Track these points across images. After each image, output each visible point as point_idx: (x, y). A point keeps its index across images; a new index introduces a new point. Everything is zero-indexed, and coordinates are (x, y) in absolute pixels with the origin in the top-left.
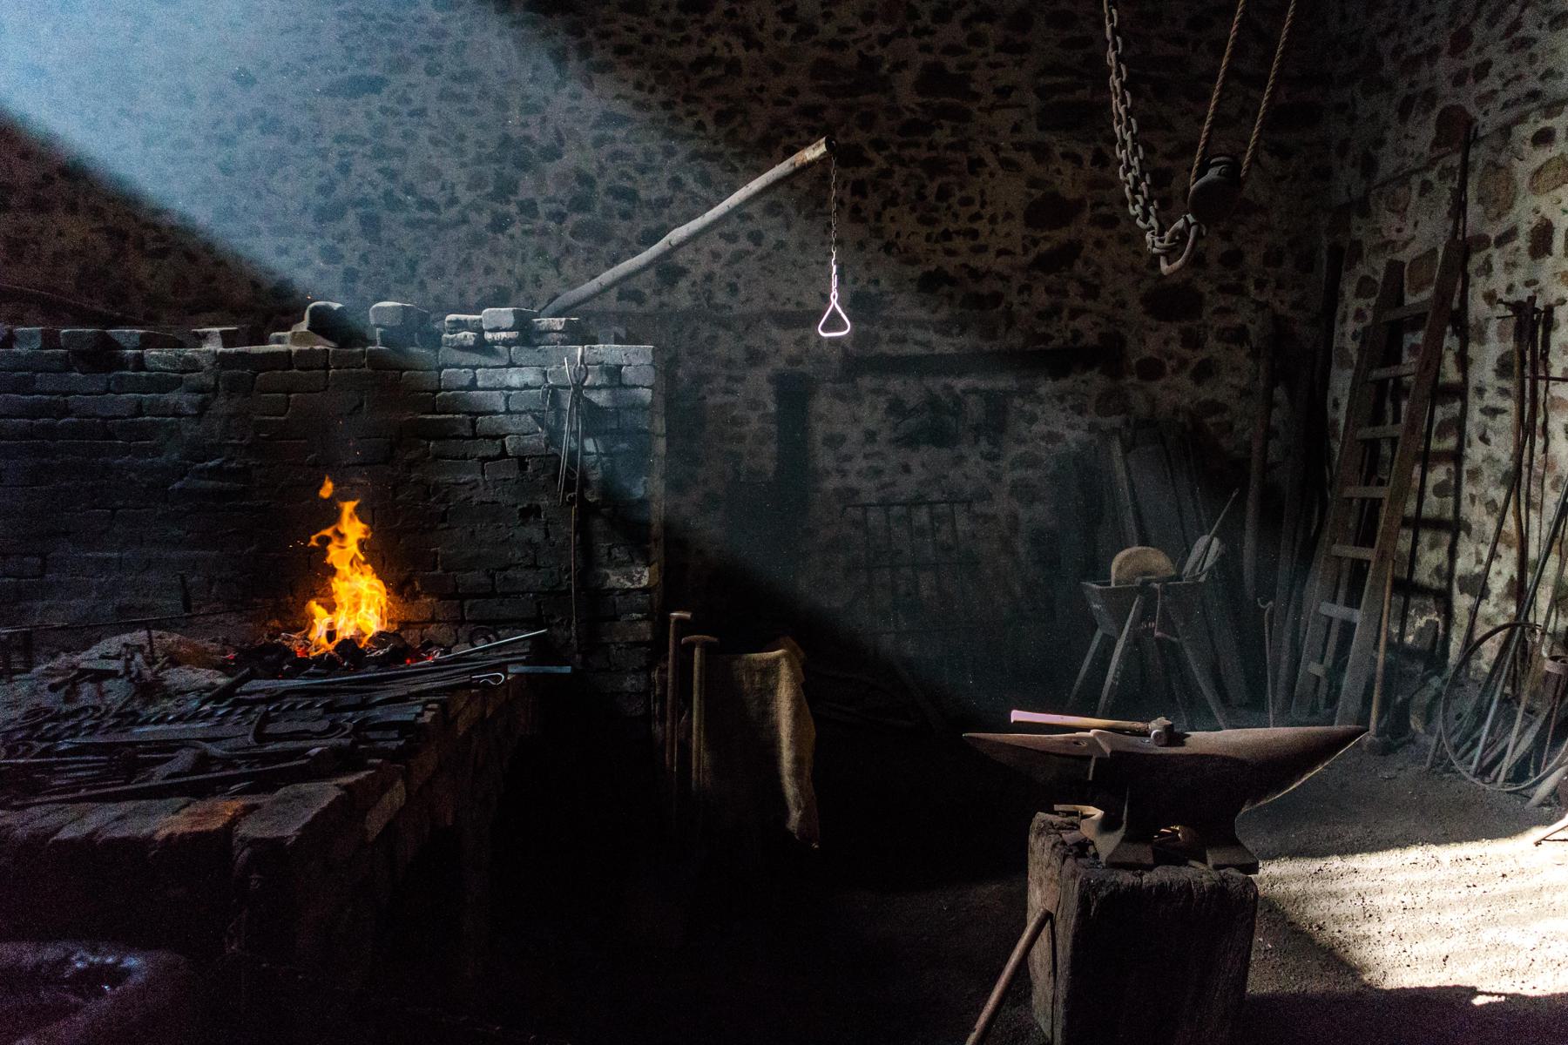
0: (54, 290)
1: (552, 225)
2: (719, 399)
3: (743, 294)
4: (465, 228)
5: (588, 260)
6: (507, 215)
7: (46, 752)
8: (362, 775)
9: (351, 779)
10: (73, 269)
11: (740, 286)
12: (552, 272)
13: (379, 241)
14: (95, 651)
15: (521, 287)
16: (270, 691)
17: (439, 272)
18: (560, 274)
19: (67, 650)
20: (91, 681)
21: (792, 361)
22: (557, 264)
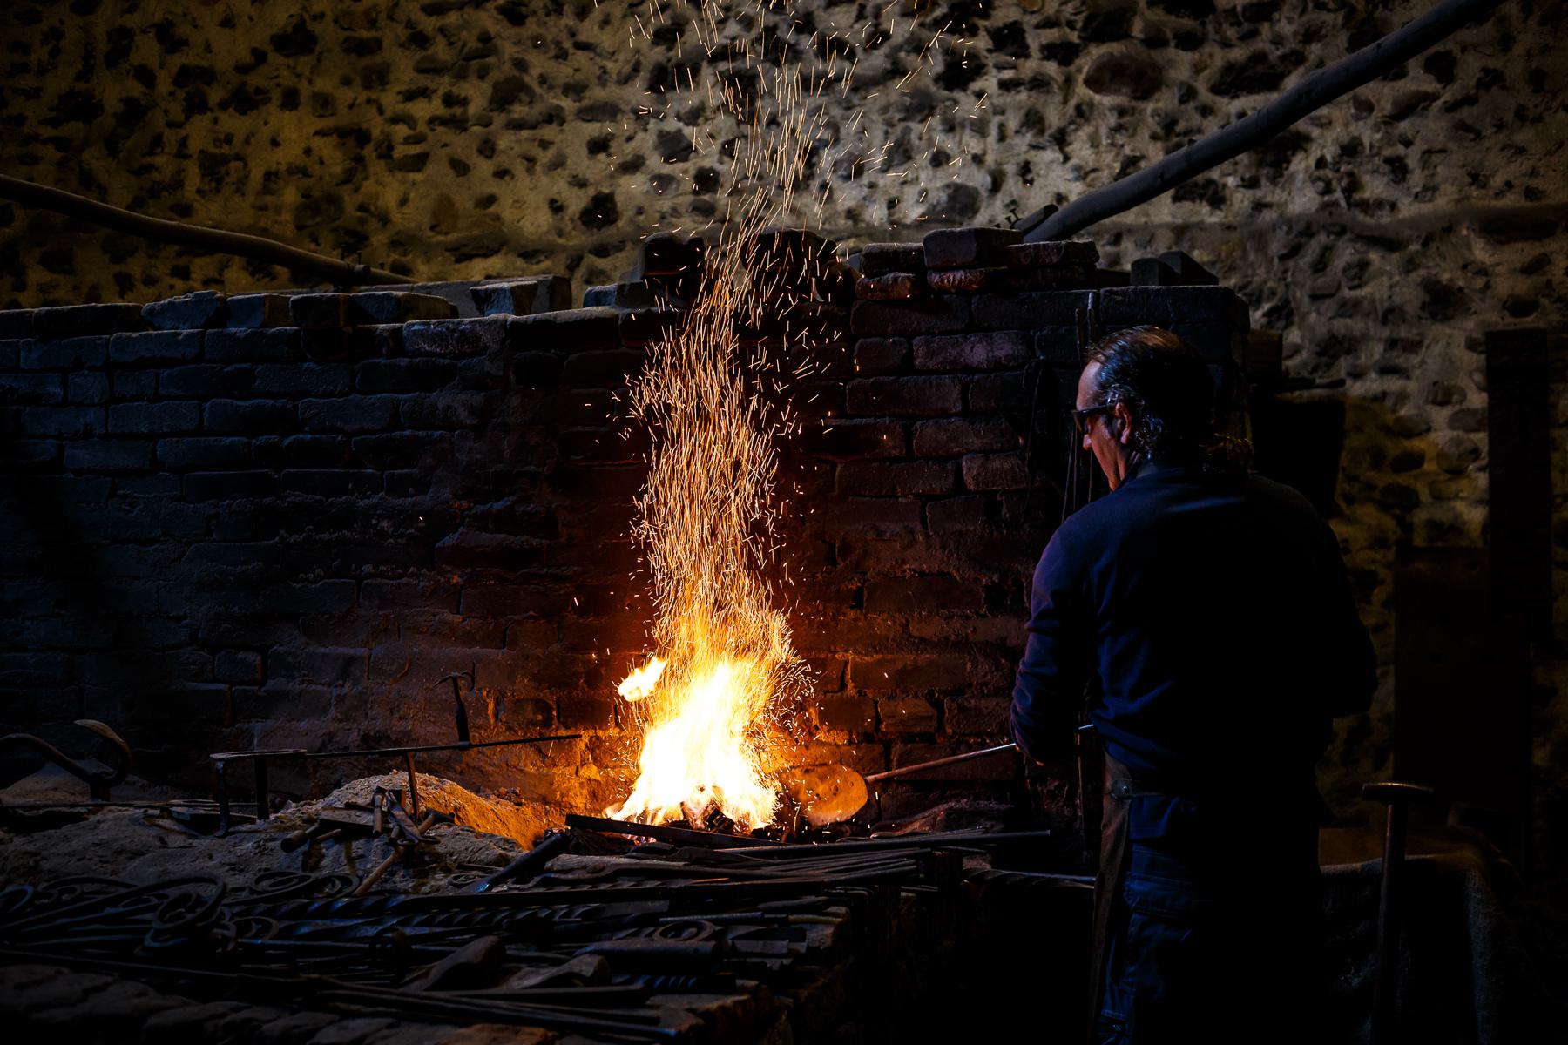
0: (264, 232)
1: (1051, 68)
2: (1372, 384)
3: (1417, 179)
4: (899, 84)
5: (1119, 128)
6: (973, 56)
7: (285, 933)
8: (729, 1001)
9: (712, 1003)
10: (290, 195)
11: (1413, 161)
12: (1051, 154)
13: (152, 26)
14: (338, 797)
15: (996, 187)
16: (597, 869)
17: (855, 169)
18: (1067, 158)
19: (297, 799)
20: (337, 839)
21: (1517, 306)
22: (1061, 139)
